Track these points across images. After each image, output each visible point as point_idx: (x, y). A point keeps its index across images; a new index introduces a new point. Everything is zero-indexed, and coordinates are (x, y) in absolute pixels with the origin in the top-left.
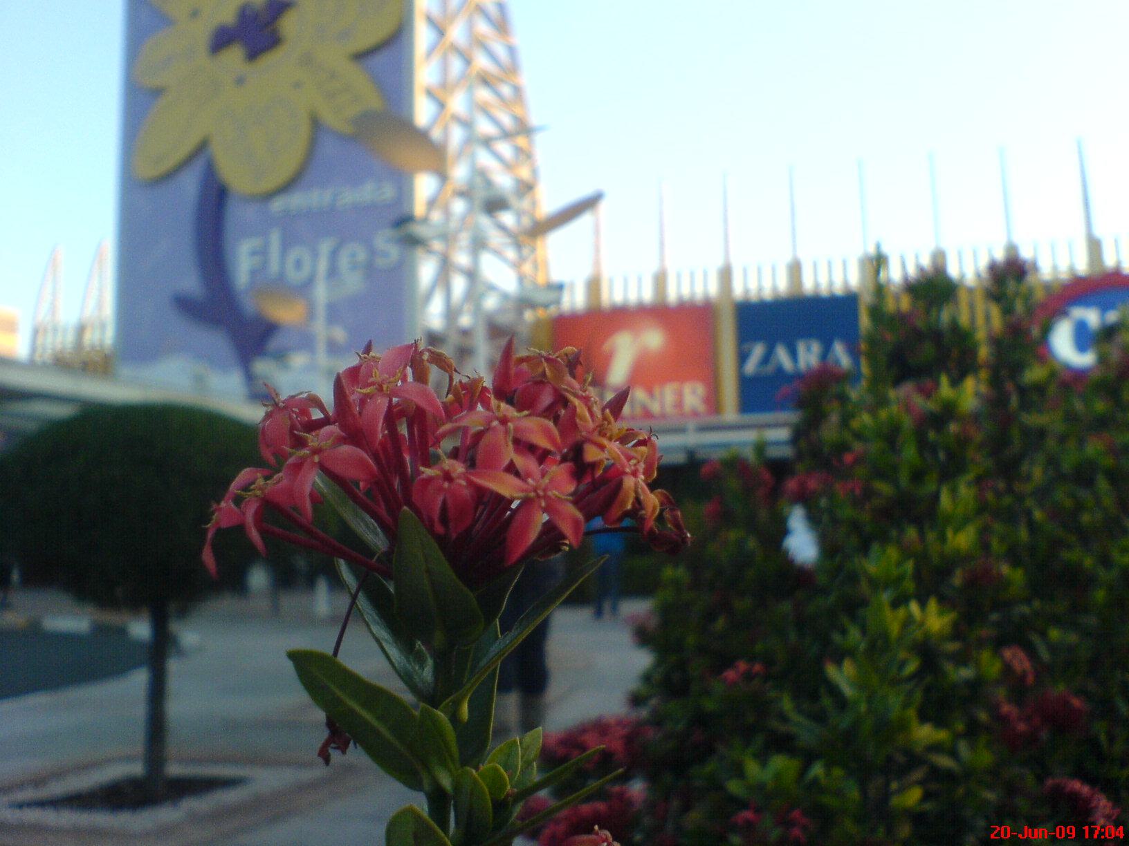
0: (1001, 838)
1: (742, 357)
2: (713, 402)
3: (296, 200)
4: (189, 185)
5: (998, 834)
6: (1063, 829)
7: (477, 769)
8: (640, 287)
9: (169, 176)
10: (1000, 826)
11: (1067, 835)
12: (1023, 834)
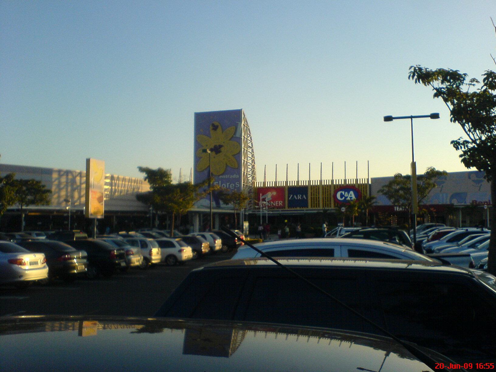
0: (440, 369)
1: (289, 197)
2: (284, 203)
3: (224, 177)
4: (206, 172)
5: (439, 367)
6: (467, 364)
7: (460, 366)
8: (270, 184)
9: (203, 171)
12: (450, 367)
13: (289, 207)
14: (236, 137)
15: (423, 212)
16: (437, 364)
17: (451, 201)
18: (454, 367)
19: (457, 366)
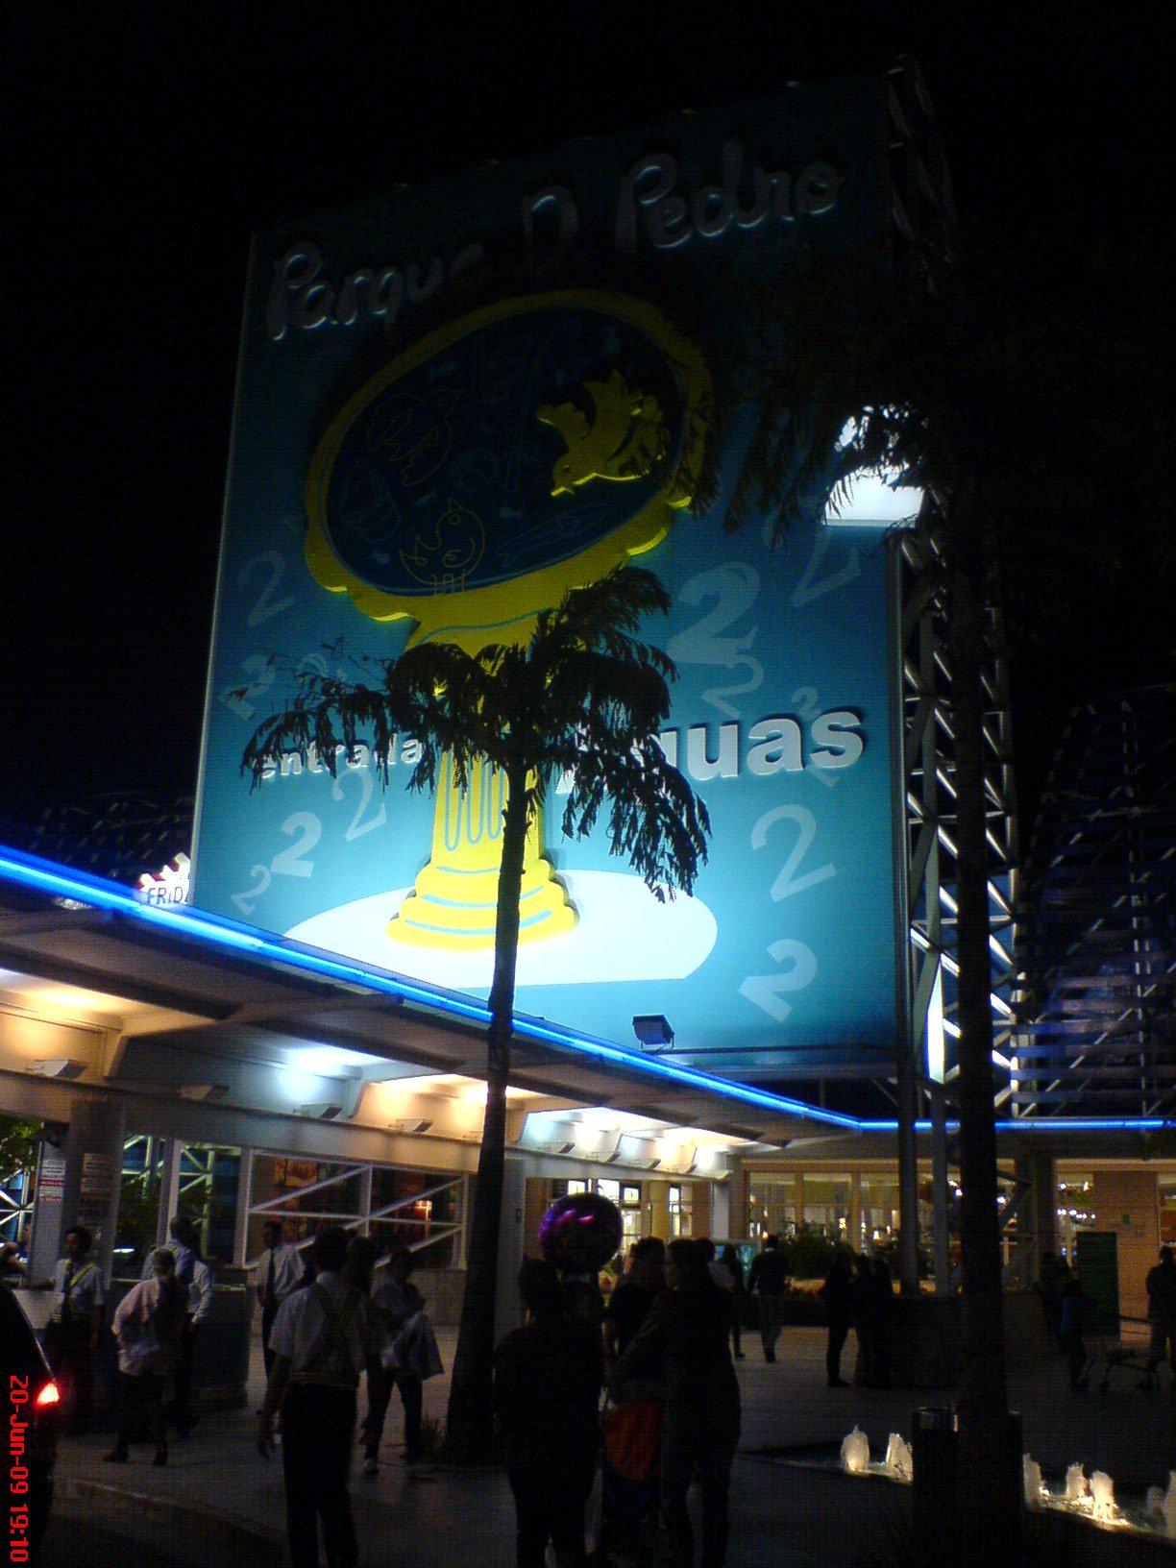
5: (17, 1387)
7: (20, 1456)
10: (11, 1428)
11: (15, 1482)
12: (16, 1421)
13: (252, 1217)
14: (268, 1287)
15: (622, 657)
16: (24, 1383)
17: (479, 658)
18: (15, 1434)
19: (18, 1445)
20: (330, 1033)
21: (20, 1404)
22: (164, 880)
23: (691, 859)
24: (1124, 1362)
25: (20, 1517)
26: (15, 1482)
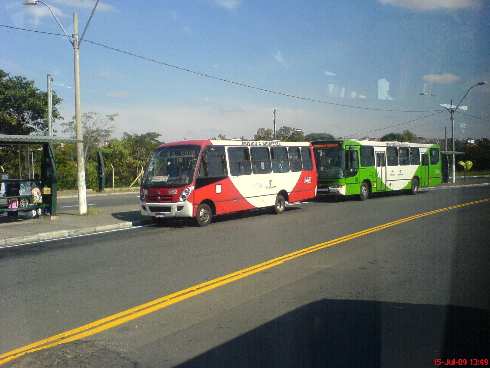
10: (449, 364)
11: (463, 363)
12: (447, 363)
20: (282, 213)
21: (455, 362)
22: (146, 210)
23: (212, 149)
24: (328, 150)
25: (485, 362)
26: (463, 363)
